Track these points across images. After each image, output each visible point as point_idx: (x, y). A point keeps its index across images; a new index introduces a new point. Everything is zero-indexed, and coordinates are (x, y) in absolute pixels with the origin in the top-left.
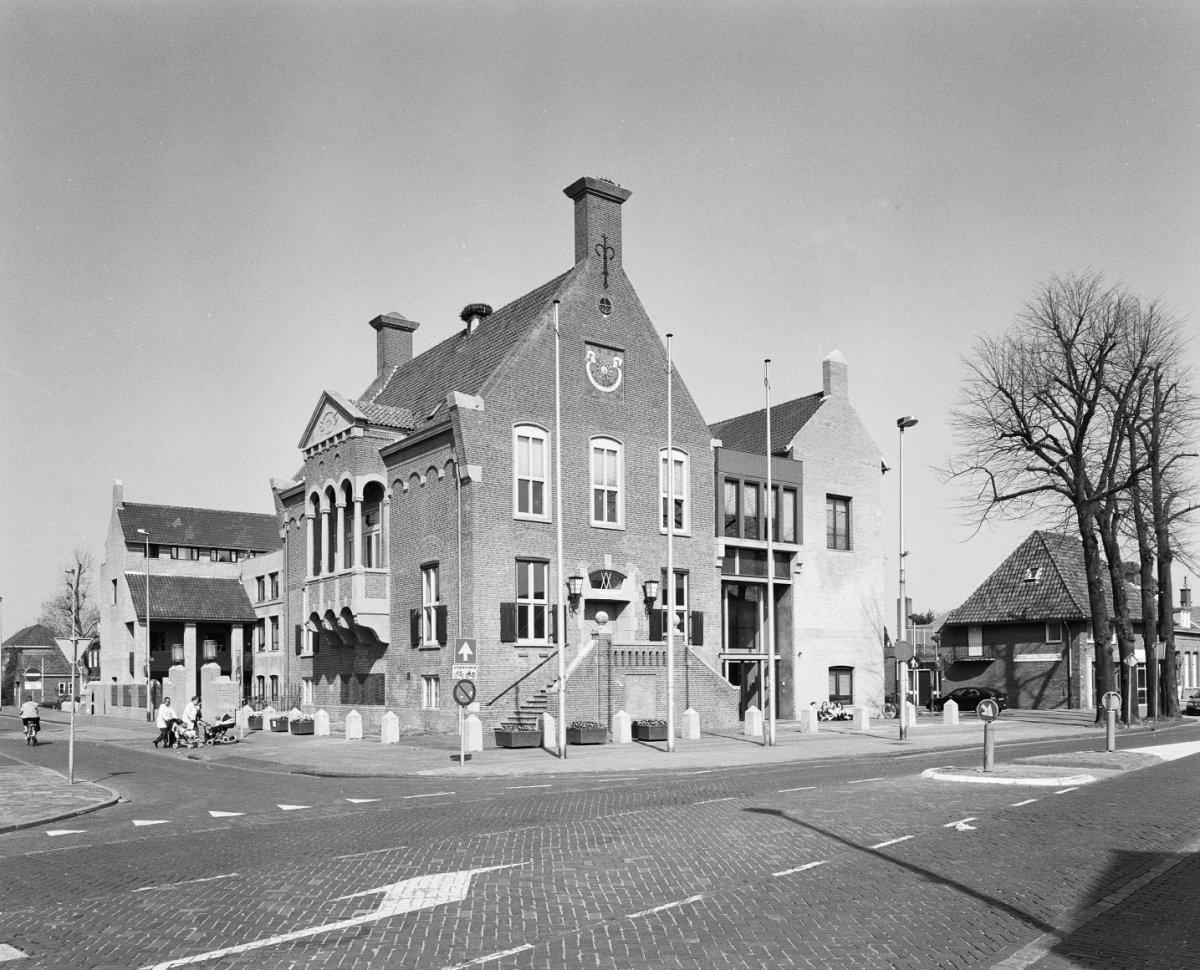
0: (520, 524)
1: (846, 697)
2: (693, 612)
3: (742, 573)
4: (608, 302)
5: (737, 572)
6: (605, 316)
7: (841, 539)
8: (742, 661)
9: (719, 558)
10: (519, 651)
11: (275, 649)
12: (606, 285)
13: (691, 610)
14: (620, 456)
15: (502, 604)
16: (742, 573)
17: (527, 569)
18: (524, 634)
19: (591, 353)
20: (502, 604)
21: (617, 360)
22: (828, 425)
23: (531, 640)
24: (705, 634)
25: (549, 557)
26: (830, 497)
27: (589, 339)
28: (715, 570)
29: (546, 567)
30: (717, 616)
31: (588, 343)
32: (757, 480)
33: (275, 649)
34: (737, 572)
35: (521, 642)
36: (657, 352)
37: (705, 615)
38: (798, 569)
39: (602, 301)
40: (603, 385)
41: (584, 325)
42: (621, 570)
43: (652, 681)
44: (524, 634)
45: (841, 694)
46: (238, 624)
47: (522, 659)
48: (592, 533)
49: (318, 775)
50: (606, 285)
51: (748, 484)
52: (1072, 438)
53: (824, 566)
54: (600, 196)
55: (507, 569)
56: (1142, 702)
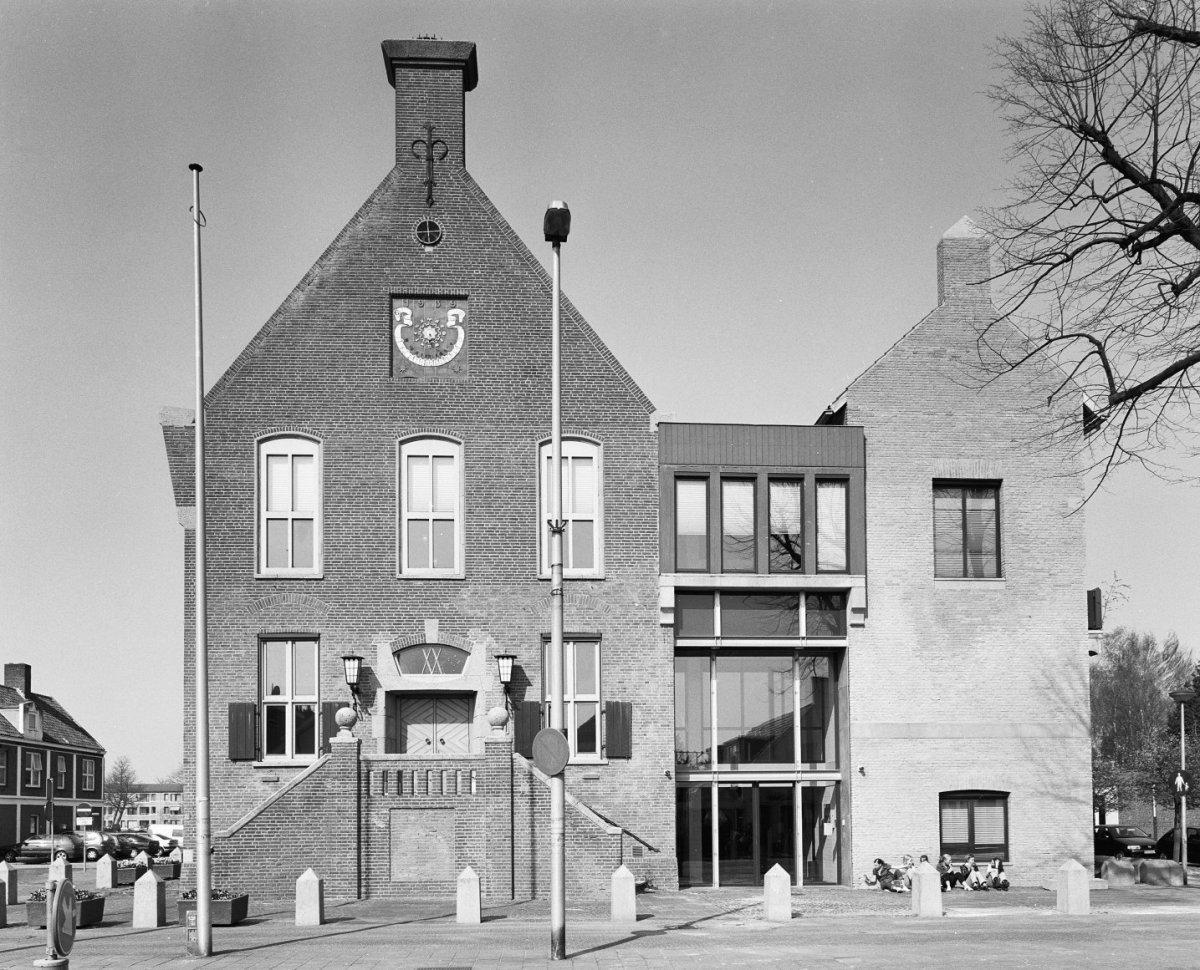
0: (268, 585)
1: (991, 849)
2: (608, 703)
3: (812, 633)
4: (433, 226)
5: (803, 633)
6: (429, 249)
7: (977, 555)
8: (755, 783)
9: (664, 610)
10: (262, 774)
11: (385, 774)
12: (430, 201)
13: (322, 701)
14: (458, 463)
15: (232, 706)
16: (812, 633)
17: (284, 648)
18: (277, 746)
19: (404, 312)
20: (232, 706)
21: (455, 314)
22: (936, 354)
23: (289, 756)
24: (635, 739)
25: (318, 630)
26: (941, 485)
27: (396, 290)
28: (660, 631)
29: (597, 647)
30: (664, 709)
31: (394, 296)
32: (800, 470)
33: (385, 774)
34: (803, 633)
35: (270, 760)
36: (534, 287)
37: (634, 708)
38: (858, 619)
39: (422, 227)
40: (428, 356)
41: (387, 270)
42: (458, 642)
43: (447, 819)
44: (277, 746)
45: (980, 840)
46: (675, 642)
47: (266, 787)
48: (400, 588)
49: (238, 951)
50: (430, 201)
51: (775, 479)
52: (205, 394)
53: (927, 609)
54: (421, 67)
55: (242, 652)
56: (810, 862)
